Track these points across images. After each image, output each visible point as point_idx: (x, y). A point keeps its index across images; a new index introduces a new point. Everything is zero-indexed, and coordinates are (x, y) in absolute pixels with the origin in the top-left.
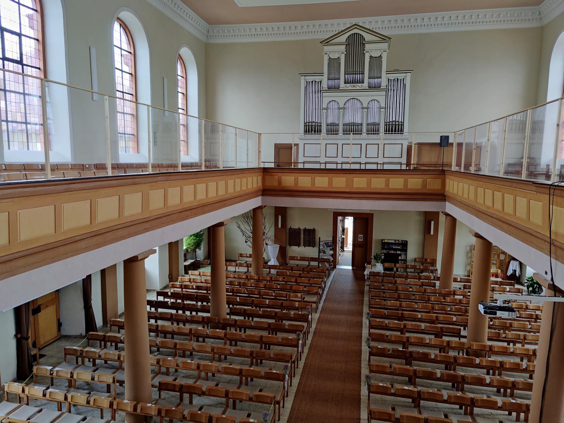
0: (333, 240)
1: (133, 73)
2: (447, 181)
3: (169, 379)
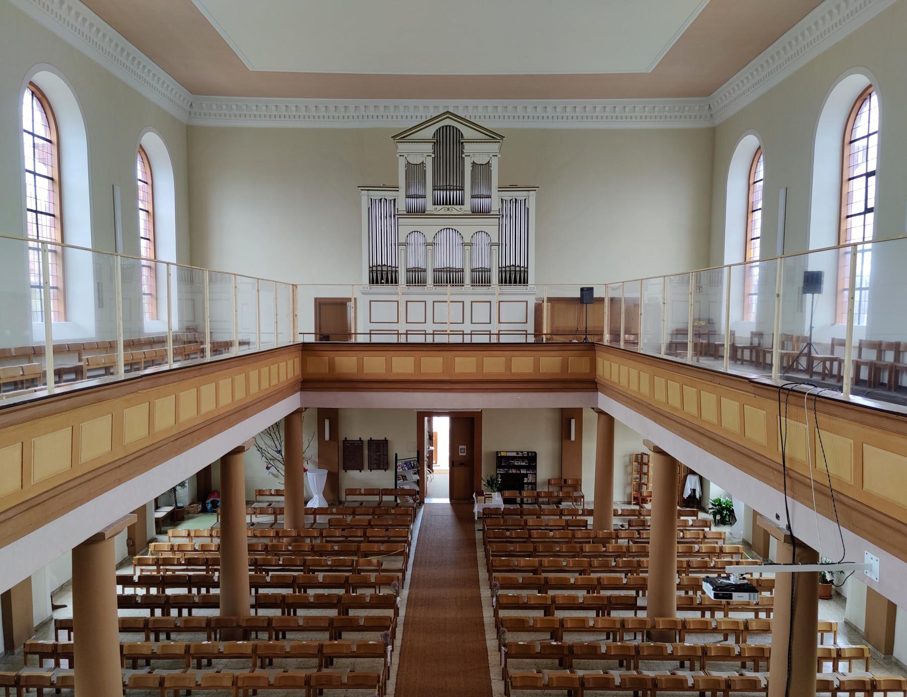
0: (418, 457)
1: (56, 178)
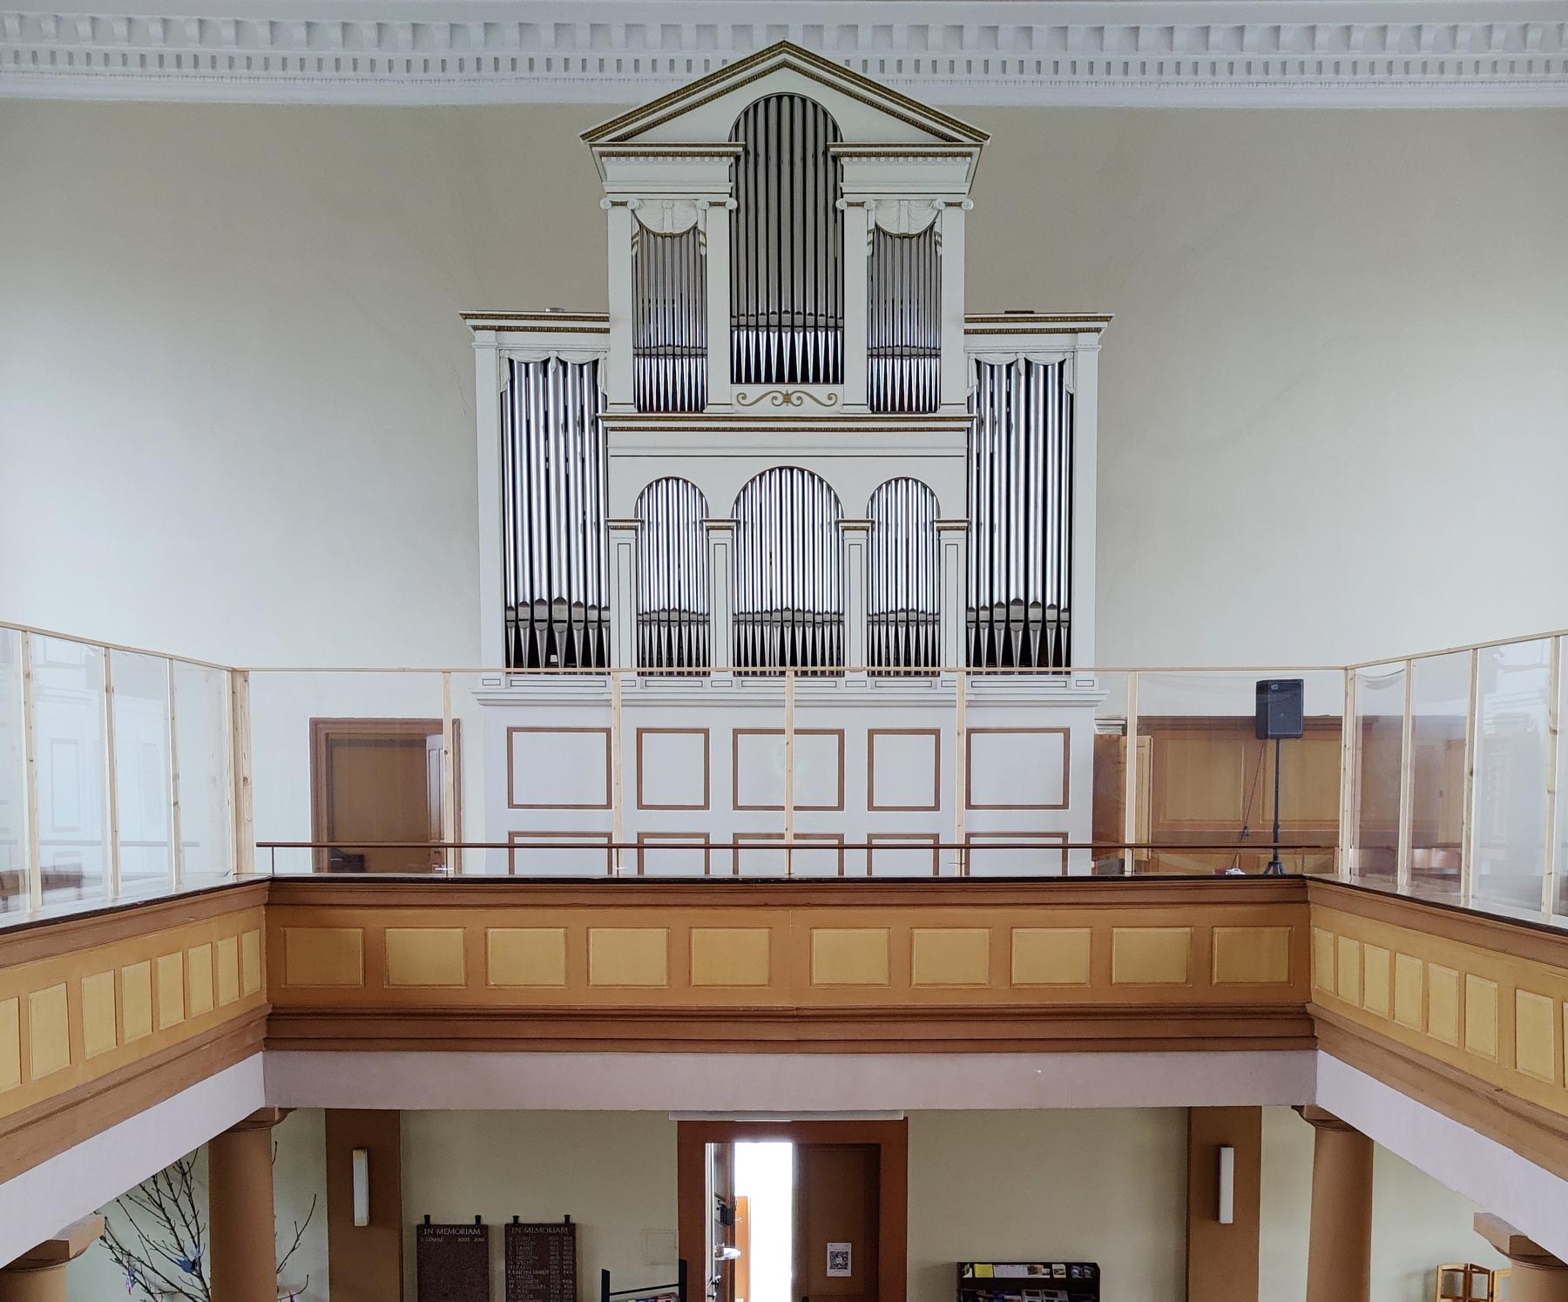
0: (682, 1284)
2: (1322, 939)
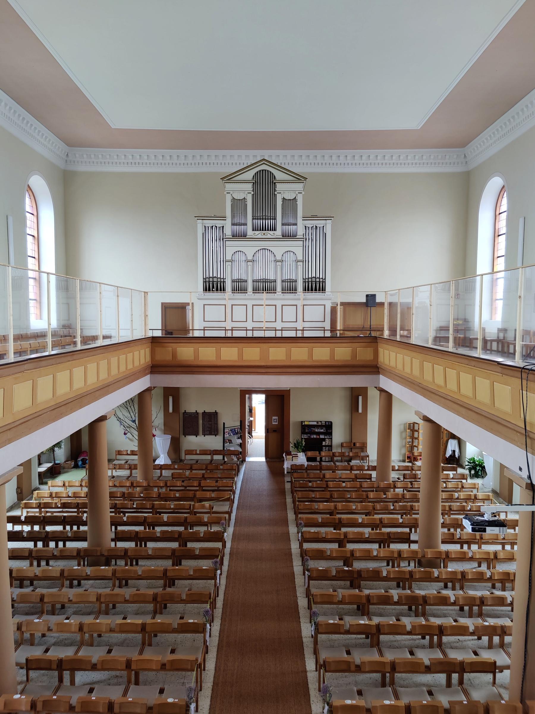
0: (241, 426)
2: (381, 350)
3: (36, 652)
